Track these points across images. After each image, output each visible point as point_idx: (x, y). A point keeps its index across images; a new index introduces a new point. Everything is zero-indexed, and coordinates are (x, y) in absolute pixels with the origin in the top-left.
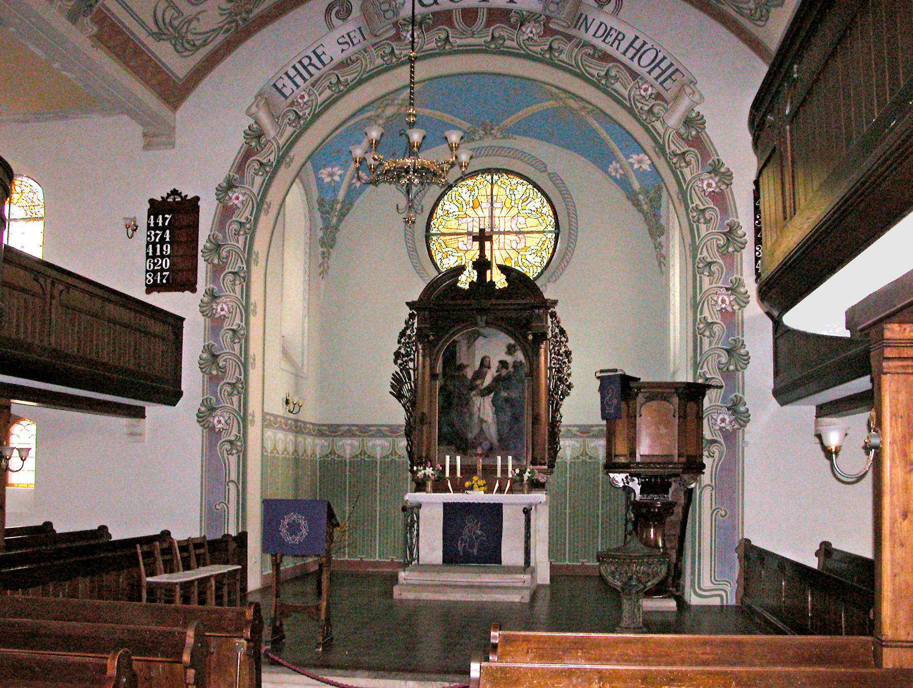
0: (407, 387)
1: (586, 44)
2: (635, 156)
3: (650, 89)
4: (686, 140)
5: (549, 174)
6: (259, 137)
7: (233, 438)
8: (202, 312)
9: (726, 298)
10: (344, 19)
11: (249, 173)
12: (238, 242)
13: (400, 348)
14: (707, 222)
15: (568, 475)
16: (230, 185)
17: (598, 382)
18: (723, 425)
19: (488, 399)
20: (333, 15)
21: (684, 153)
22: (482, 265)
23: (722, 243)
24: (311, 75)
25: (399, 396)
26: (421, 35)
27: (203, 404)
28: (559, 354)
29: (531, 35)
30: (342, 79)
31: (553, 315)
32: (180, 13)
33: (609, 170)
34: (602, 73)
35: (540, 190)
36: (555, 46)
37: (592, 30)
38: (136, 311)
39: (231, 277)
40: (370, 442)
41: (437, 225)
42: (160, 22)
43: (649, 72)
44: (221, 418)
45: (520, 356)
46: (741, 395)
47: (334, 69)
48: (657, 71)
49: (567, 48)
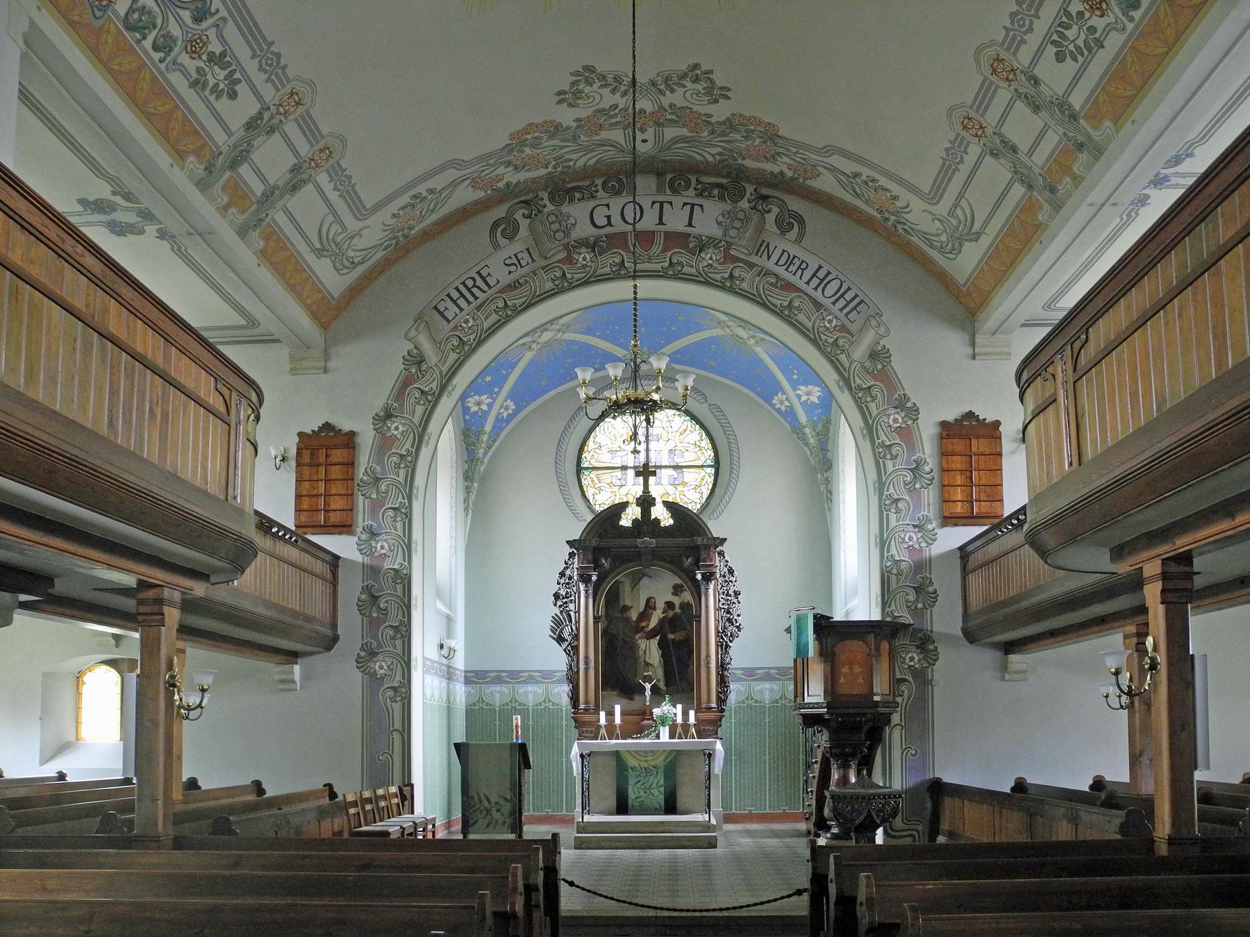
1: (768, 273)
2: (803, 388)
6: (420, 363)
7: (396, 685)
8: (360, 550)
14: (894, 458)
16: (388, 415)
19: (654, 642)
20: (499, 234)
21: (869, 388)
22: (646, 502)
24: (476, 298)
25: (560, 640)
27: (362, 649)
28: (728, 594)
31: (721, 554)
33: (774, 401)
34: (786, 304)
36: (736, 274)
37: (774, 258)
39: (391, 513)
40: (522, 689)
43: (834, 303)
45: (687, 596)
48: (842, 302)
49: (748, 276)
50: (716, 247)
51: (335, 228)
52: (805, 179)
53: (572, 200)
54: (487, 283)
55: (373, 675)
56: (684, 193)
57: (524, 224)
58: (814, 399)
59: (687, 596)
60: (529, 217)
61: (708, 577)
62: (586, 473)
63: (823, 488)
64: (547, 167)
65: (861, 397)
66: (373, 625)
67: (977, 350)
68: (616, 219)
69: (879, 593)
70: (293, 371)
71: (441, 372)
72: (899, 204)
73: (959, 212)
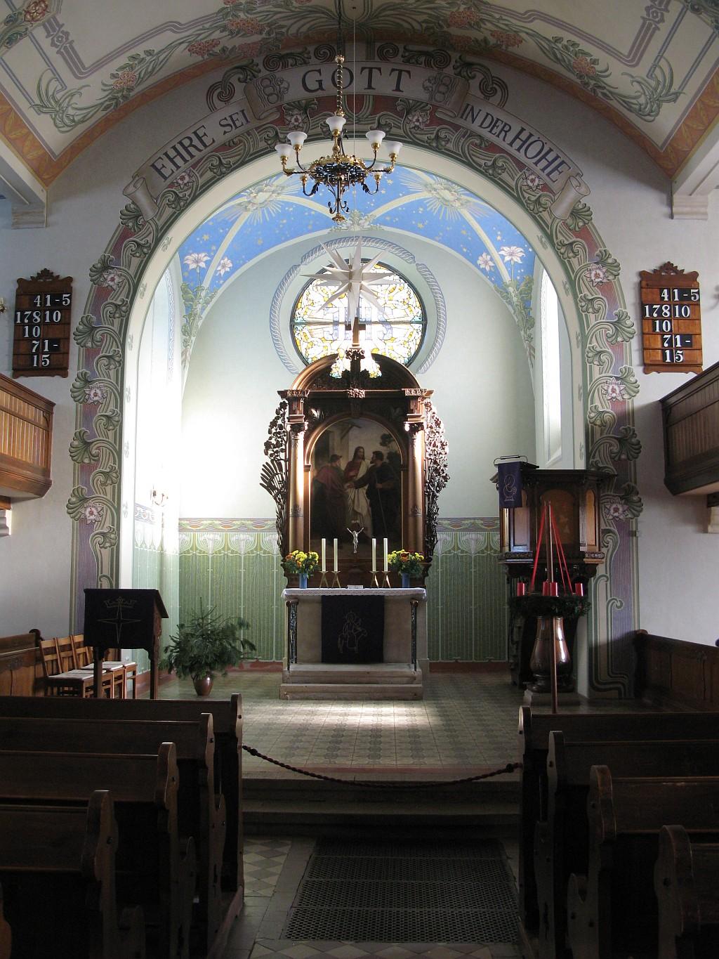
0: (278, 478)
1: (473, 134)
3: (537, 180)
4: (573, 231)
5: (417, 265)
8: (74, 397)
9: (616, 387)
10: (227, 101)
11: (125, 254)
12: (113, 325)
13: (271, 438)
15: (440, 570)
16: (105, 266)
17: (496, 470)
18: (616, 514)
19: (363, 492)
21: (571, 244)
23: (611, 332)
24: (192, 156)
25: (269, 487)
26: (306, 120)
27: (73, 495)
28: (434, 446)
29: (418, 124)
30: (224, 161)
32: (64, 87)
33: (479, 262)
34: (490, 163)
35: (406, 280)
37: (479, 120)
38: (13, 394)
39: (105, 361)
41: (301, 315)
42: (43, 92)
43: (536, 164)
44: (93, 509)
45: (395, 446)
46: (633, 485)
47: (216, 150)
48: (543, 163)
50: (423, 110)
51: (54, 85)
52: (507, 46)
53: (285, 66)
54: (202, 142)
55: (83, 520)
56: (392, 60)
57: (239, 88)
58: (517, 259)
59: (395, 446)
60: (245, 81)
61: (417, 427)
62: (300, 328)
63: (526, 344)
64: (261, 33)
65: (564, 252)
66: (85, 470)
67: (674, 209)
68: (327, 83)
69: (583, 443)
70: (16, 225)
71: (157, 225)
72: (598, 68)
73: (658, 72)
